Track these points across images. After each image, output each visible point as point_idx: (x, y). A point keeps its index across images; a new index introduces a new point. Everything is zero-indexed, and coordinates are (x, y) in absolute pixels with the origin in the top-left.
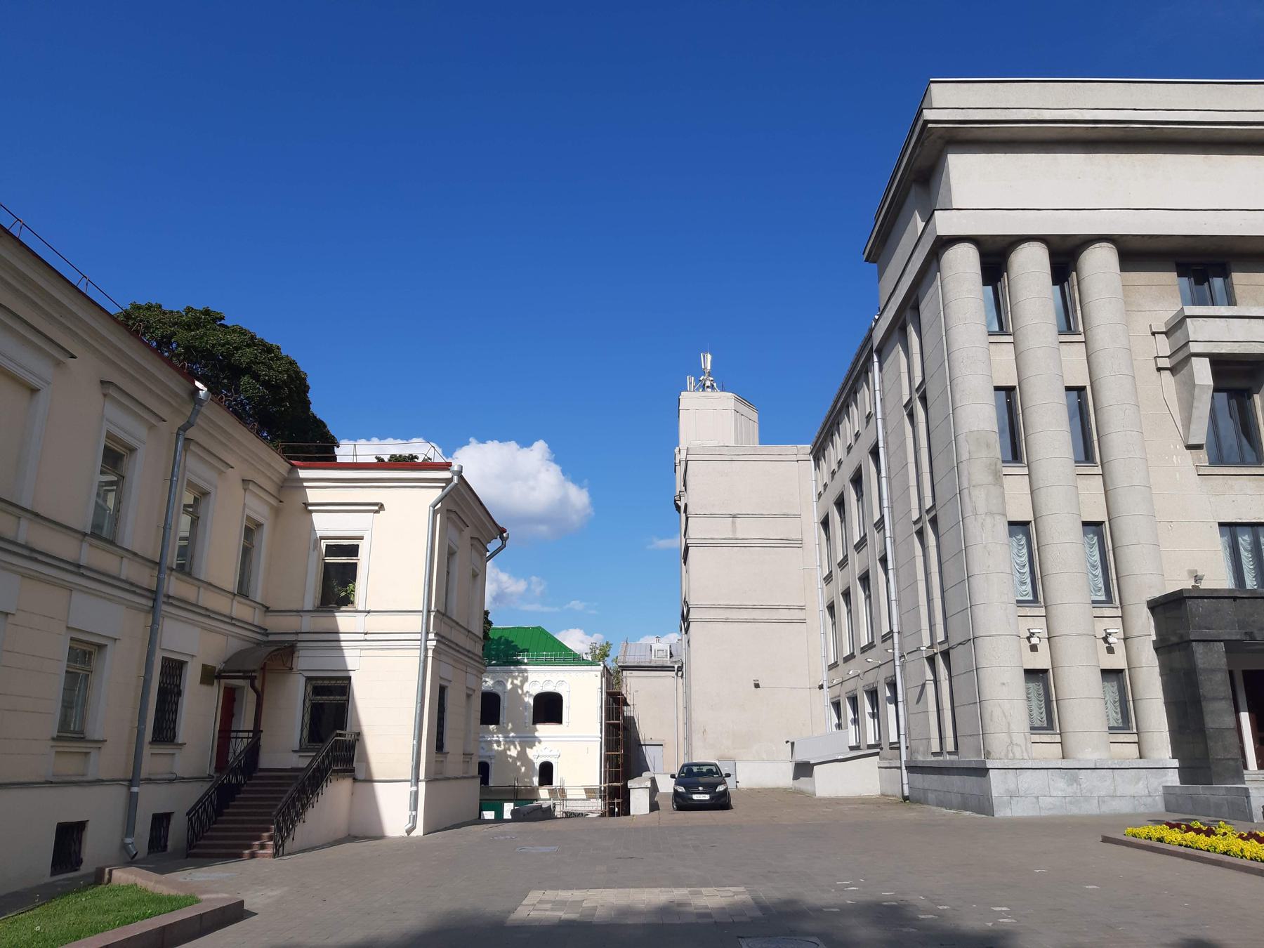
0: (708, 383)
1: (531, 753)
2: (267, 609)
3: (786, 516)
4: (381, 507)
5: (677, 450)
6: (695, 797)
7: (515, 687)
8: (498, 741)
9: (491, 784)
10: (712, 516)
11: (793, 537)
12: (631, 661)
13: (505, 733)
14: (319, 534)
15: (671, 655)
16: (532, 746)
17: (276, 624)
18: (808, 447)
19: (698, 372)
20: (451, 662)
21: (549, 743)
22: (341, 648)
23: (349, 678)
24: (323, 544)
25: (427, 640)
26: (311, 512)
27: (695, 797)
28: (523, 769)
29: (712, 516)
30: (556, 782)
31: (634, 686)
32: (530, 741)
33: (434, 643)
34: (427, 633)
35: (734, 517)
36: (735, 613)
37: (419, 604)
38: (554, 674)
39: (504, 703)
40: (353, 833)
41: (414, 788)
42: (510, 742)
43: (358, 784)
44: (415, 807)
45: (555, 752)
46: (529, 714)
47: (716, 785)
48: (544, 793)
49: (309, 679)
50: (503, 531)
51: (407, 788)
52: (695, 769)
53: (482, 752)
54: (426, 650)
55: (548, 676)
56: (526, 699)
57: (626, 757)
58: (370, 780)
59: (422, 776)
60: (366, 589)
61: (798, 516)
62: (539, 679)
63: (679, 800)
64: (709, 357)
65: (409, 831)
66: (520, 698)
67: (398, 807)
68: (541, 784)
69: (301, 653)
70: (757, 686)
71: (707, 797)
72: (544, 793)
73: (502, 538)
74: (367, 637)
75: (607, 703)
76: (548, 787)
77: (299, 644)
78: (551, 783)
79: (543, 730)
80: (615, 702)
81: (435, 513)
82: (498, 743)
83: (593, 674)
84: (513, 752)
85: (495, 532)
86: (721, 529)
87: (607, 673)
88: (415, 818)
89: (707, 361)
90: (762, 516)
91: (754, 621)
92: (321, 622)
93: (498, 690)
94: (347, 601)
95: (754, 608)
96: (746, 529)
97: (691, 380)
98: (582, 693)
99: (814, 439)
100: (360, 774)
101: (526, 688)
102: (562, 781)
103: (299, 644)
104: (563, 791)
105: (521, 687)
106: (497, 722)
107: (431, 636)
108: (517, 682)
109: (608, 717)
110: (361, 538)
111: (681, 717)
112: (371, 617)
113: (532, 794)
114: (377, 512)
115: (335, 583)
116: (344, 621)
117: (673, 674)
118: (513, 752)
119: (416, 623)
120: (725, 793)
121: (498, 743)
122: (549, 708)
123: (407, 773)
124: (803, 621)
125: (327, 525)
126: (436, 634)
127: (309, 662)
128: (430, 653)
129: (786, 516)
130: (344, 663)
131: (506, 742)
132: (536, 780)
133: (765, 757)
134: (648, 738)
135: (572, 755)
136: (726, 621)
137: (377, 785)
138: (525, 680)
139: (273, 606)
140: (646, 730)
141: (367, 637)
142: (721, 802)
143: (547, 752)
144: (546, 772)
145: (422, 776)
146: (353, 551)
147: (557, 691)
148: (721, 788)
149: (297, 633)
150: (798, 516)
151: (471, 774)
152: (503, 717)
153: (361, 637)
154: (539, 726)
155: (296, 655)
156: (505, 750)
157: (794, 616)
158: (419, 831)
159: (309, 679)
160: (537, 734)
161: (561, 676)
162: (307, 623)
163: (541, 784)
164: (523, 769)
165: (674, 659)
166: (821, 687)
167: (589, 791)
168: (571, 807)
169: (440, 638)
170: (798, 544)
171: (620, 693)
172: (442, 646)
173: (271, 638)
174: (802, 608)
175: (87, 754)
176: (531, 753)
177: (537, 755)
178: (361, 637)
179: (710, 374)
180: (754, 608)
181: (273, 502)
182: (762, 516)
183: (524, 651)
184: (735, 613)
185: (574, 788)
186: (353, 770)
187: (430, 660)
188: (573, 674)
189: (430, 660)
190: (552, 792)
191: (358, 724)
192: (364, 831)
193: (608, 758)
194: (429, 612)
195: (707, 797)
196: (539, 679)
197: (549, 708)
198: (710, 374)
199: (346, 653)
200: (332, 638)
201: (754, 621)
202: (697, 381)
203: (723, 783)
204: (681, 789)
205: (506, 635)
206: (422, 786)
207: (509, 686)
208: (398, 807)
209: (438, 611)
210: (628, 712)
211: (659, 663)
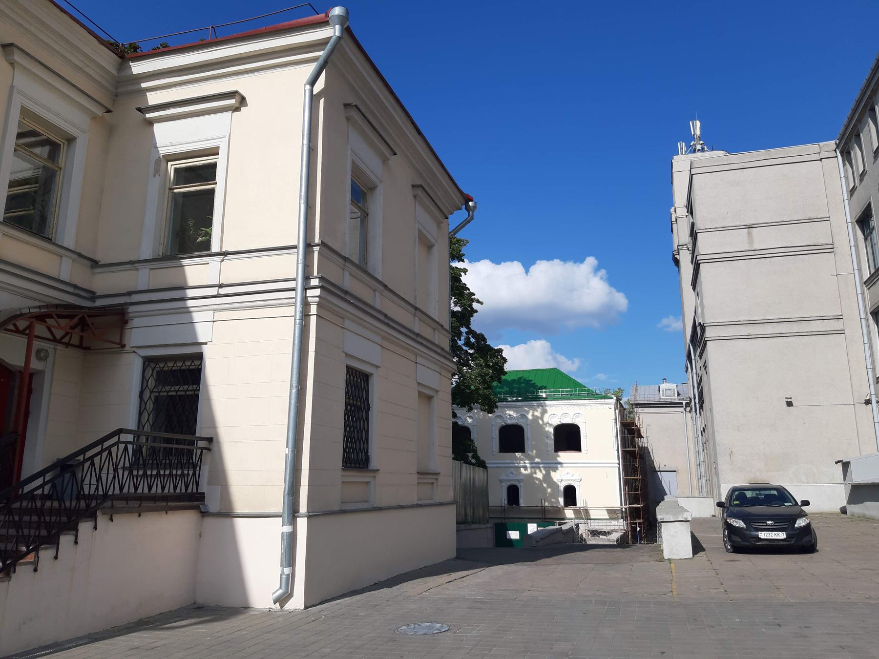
0: (699, 147)
1: (555, 476)
2: (95, 264)
3: (812, 220)
4: (243, 101)
5: (672, 210)
6: (763, 535)
7: (536, 418)
8: (524, 466)
9: (522, 503)
10: (724, 229)
11: (822, 242)
12: (641, 399)
13: (531, 458)
14: (162, 151)
15: (679, 394)
16: (555, 469)
17: (106, 283)
18: (832, 144)
19: (688, 138)
20: (378, 339)
21: (569, 468)
22: (187, 311)
23: (200, 357)
24: (171, 167)
25: (305, 289)
26: (150, 123)
27: (763, 535)
28: (549, 490)
29: (724, 229)
30: (580, 503)
31: (646, 420)
32: (554, 465)
33: (317, 292)
34: (307, 278)
35: (750, 227)
36: (752, 329)
37: (293, 234)
38: (571, 408)
39: (528, 434)
40: (200, 600)
41: (288, 529)
42: (535, 466)
43: (209, 521)
44: (289, 559)
45: (576, 477)
46: (551, 442)
47: (793, 518)
48: (569, 513)
49: (148, 361)
50: (468, 199)
51: (277, 528)
52: (749, 494)
53: (511, 477)
54: (306, 304)
55: (565, 410)
56: (547, 429)
57: (644, 481)
58: (228, 514)
59: (303, 508)
60: (229, 225)
61: (827, 219)
62: (557, 412)
63: (737, 539)
64: (698, 123)
65: (283, 600)
66: (541, 428)
67: (265, 559)
68: (567, 504)
69: (135, 322)
70: (790, 404)
71: (782, 535)
72: (569, 513)
73: (468, 208)
74: (223, 291)
75: (622, 432)
76: (573, 508)
77: (131, 309)
78: (575, 504)
79: (565, 457)
80: (629, 432)
81: (314, 99)
82: (525, 468)
83: (607, 406)
84: (539, 475)
85: (457, 199)
86: (737, 242)
87: (619, 406)
88: (289, 581)
89: (696, 128)
90: (783, 223)
91: (781, 336)
92: (163, 276)
93: (521, 422)
94: (203, 248)
95: (780, 321)
96: (764, 239)
97: (681, 146)
98: (598, 422)
99: (841, 130)
100: (212, 505)
101: (546, 418)
102: (585, 502)
103: (131, 309)
104: (586, 511)
105: (542, 418)
106: (522, 449)
107: (315, 282)
108: (538, 414)
109: (626, 473)
110: (215, 152)
111: (691, 446)
112: (231, 263)
113: (556, 515)
114: (237, 109)
115: (191, 223)
116: (197, 271)
117: (682, 409)
118: (539, 475)
119: (289, 266)
120: (808, 529)
121: (525, 468)
122: (568, 438)
123: (277, 501)
124: (841, 332)
125: (172, 137)
126: (322, 279)
127: (146, 334)
128: (314, 309)
129: (812, 220)
130: (194, 333)
131: (532, 467)
132: (561, 501)
133: (805, 481)
134: (662, 465)
135: (594, 480)
136: (748, 337)
137: (240, 523)
138: (544, 412)
139: (102, 257)
140: (659, 459)
141: (223, 291)
142: (802, 543)
143: (569, 477)
144: (570, 494)
145: (303, 508)
146: (208, 173)
147: (574, 422)
148: (801, 523)
149: (129, 294)
150: (827, 219)
151: (439, 497)
152: (528, 443)
153: (214, 291)
154: (561, 454)
155: (129, 325)
156: (531, 474)
157: (831, 327)
158: (297, 602)
159: (148, 361)
160: (559, 459)
161: (577, 409)
162: (143, 278)
163: (567, 504)
164: (549, 490)
165: (681, 397)
166: (868, 402)
167: (611, 511)
168: (595, 526)
169: (327, 285)
170: (830, 249)
171: (633, 424)
172: (330, 297)
173: (99, 303)
174: (838, 319)
175: (368, 483)
176: (555, 476)
177: (561, 478)
178: (214, 291)
179: (700, 138)
180: (780, 321)
181: (99, 111)
182: (783, 223)
183: (541, 388)
184: (752, 329)
185: (598, 509)
186: (201, 497)
187: (313, 320)
188: (588, 407)
189: (313, 320)
190: (577, 512)
191: (213, 426)
192: (211, 602)
193: (627, 482)
194: (309, 246)
195: (782, 535)
196: (557, 412)
197: (568, 438)
198: (700, 138)
199: (197, 317)
200: (176, 294)
201: (781, 336)
202: (688, 146)
203: (802, 515)
204: (739, 523)
205: (526, 376)
206: (302, 524)
207: (530, 417)
208: (265, 559)
209: (323, 244)
210: (644, 443)
211: (669, 401)
